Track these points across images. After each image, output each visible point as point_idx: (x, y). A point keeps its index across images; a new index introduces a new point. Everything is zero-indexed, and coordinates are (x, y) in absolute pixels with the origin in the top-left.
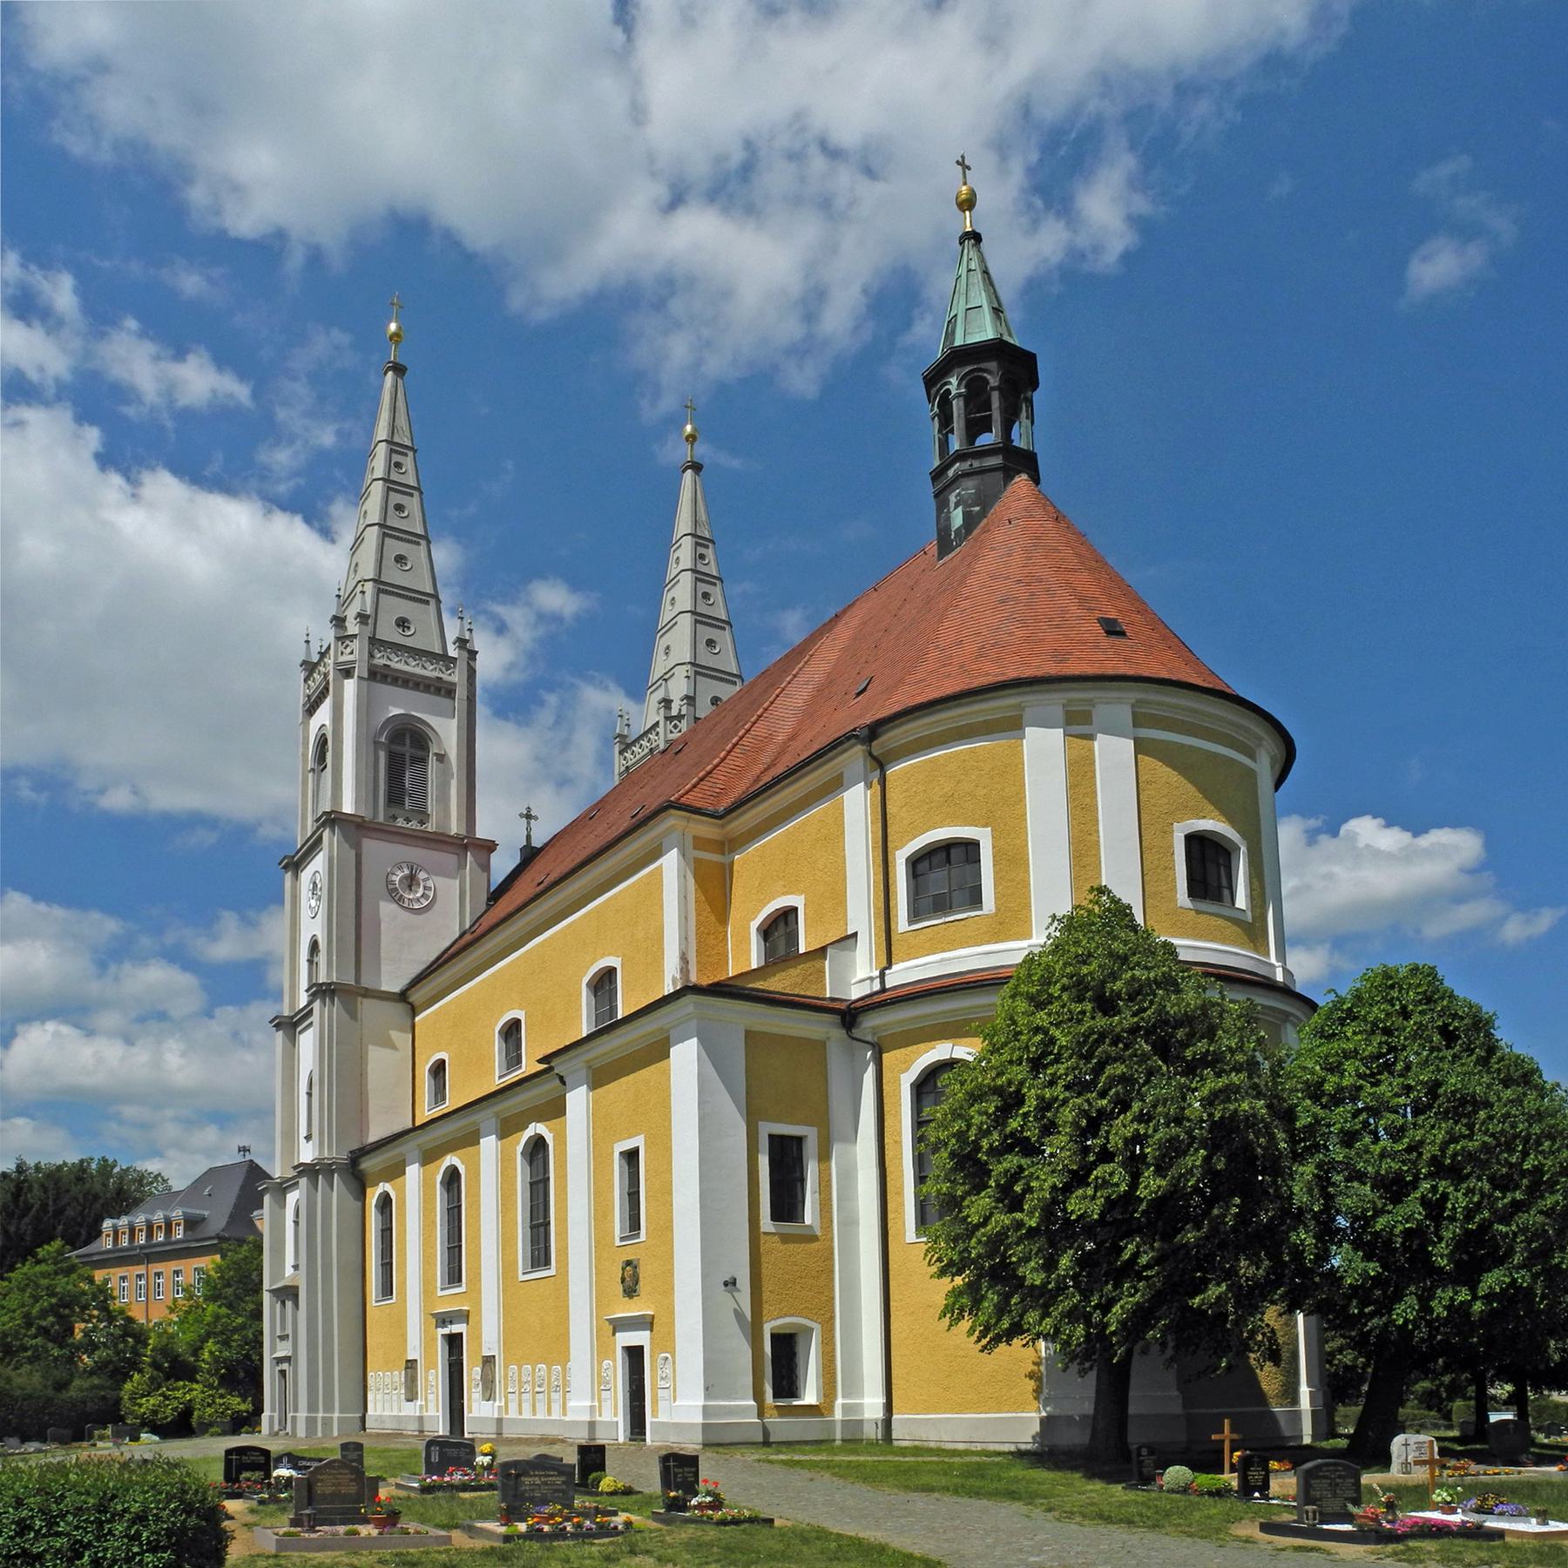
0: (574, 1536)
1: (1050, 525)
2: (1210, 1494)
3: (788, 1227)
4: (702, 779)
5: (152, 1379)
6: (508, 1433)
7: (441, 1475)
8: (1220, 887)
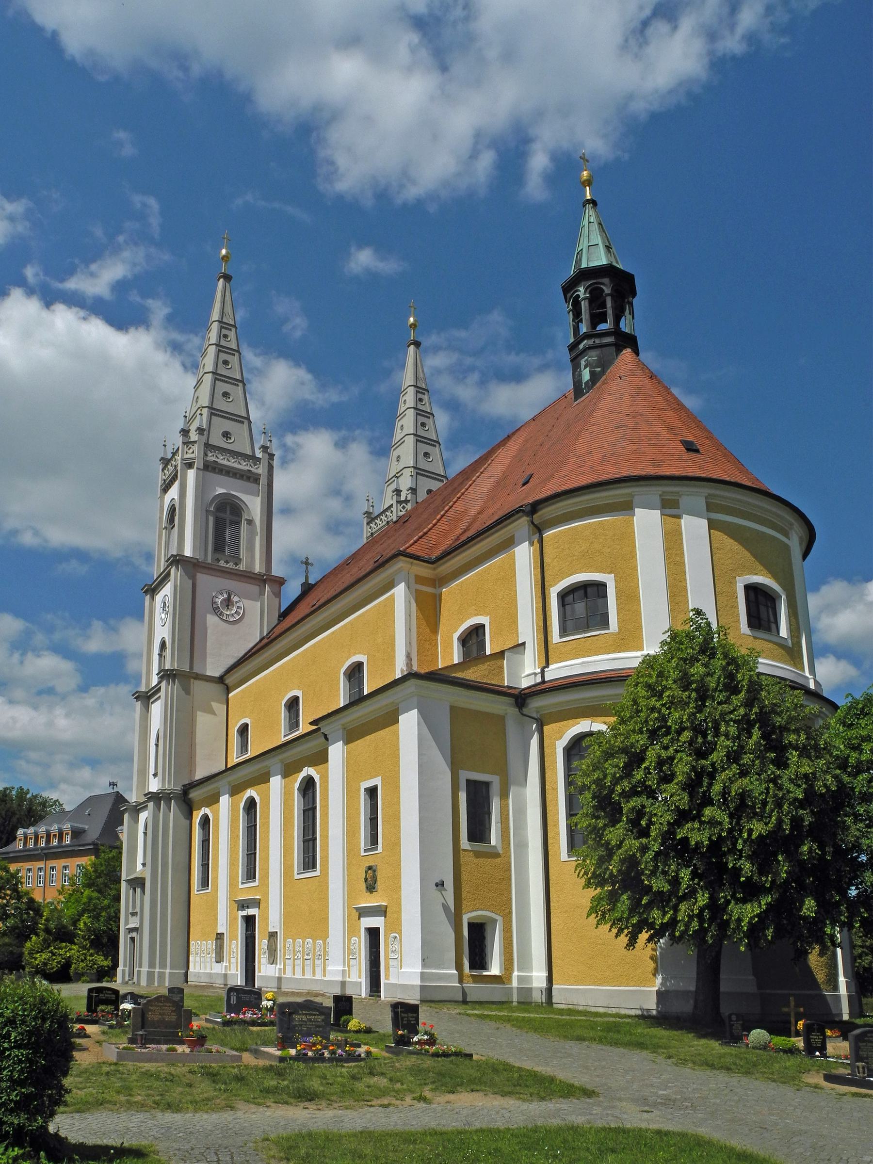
0: (330, 1060)
1: (647, 380)
2: (785, 1051)
3: (479, 846)
4: (421, 537)
5: (44, 940)
6: (285, 988)
7: (237, 1013)
8: (769, 621)
